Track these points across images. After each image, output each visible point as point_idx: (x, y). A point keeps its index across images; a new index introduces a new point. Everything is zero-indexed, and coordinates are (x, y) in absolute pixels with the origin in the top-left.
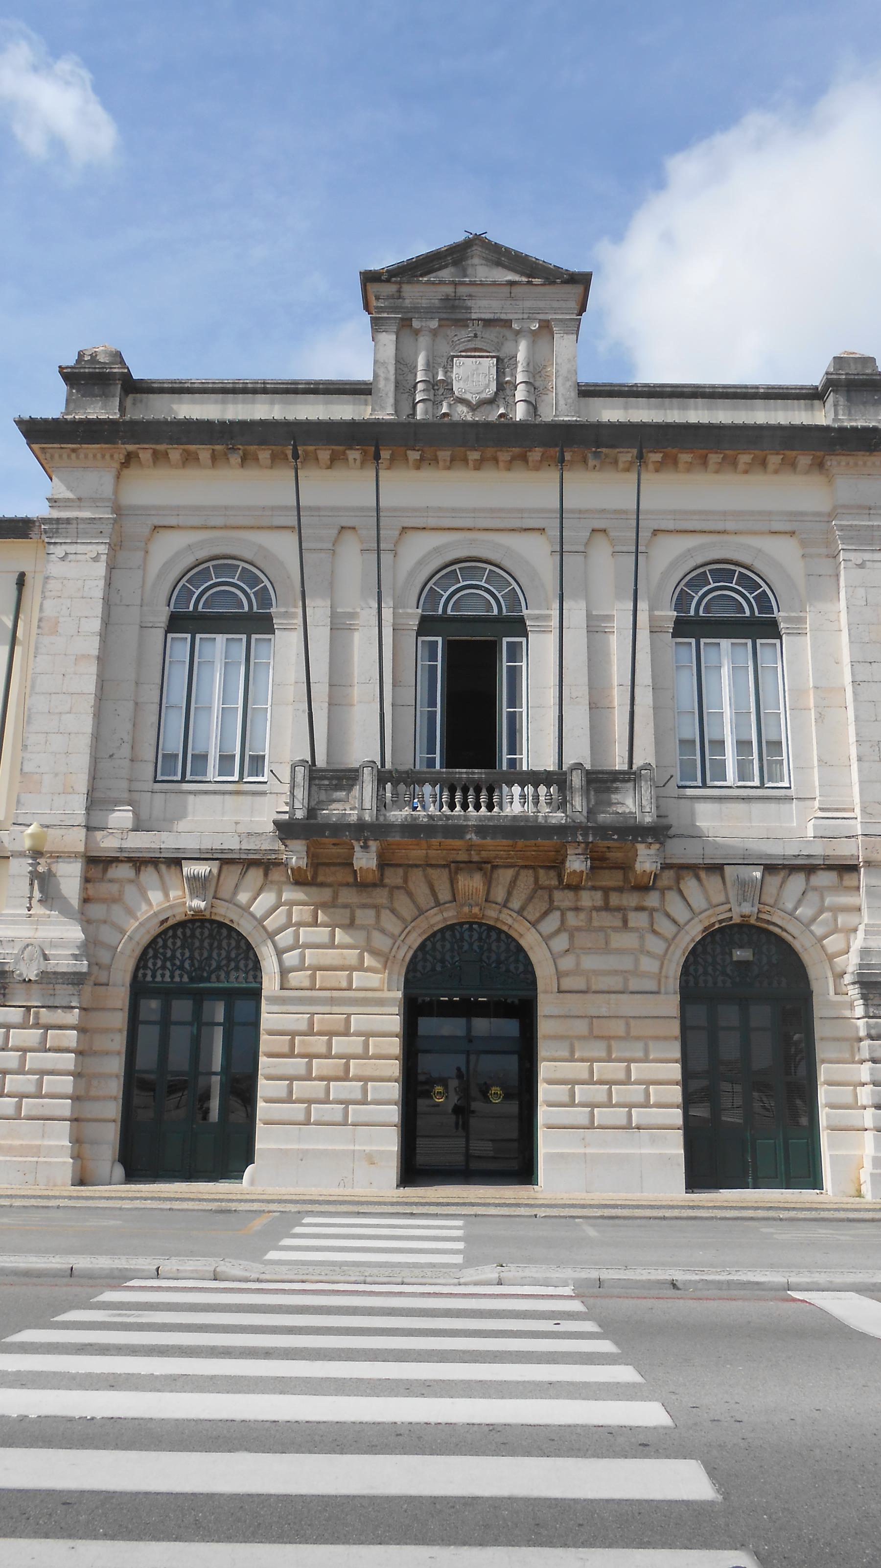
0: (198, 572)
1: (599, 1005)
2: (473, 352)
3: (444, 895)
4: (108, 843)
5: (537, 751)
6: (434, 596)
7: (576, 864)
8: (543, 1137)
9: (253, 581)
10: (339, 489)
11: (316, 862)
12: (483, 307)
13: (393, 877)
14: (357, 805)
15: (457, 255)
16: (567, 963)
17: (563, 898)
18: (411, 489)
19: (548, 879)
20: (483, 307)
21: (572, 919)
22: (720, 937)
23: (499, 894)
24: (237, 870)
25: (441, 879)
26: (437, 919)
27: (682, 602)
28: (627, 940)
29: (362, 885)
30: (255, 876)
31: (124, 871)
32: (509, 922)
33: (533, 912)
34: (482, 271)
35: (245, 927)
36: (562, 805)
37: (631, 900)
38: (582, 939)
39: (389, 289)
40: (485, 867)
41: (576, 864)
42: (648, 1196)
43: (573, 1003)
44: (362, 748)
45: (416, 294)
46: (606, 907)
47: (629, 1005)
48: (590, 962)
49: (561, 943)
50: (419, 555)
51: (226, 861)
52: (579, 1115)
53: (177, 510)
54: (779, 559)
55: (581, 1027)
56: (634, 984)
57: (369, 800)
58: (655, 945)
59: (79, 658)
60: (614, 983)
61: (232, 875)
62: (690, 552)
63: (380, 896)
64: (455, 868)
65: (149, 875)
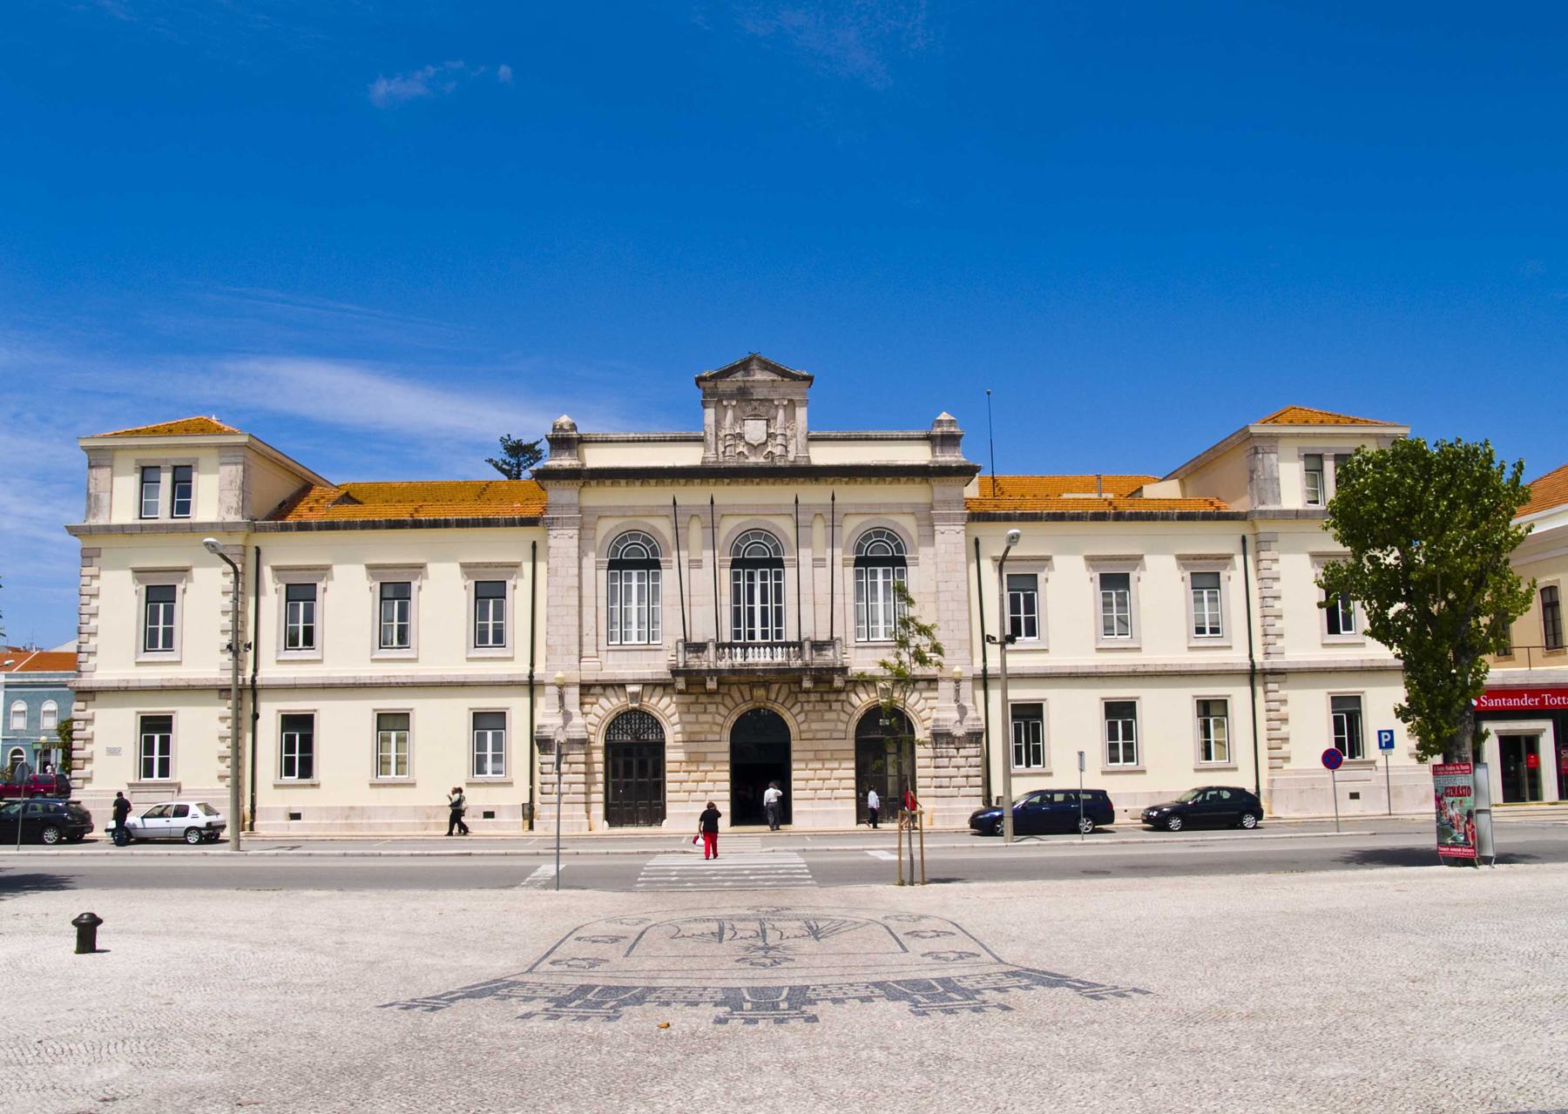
0: (745, 536)
1: (818, 745)
2: (756, 417)
3: (747, 697)
4: (589, 676)
5: (790, 635)
6: (738, 548)
7: (807, 684)
8: (794, 803)
9: (649, 542)
10: (694, 495)
11: (688, 684)
12: (759, 393)
13: (724, 689)
14: (708, 660)
15: (745, 366)
16: (804, 727)
17: (802, 697)
18: (727, 494)
19: (795, 688)
20: (759, 393)
21: (806, 707)
22: (873, 713)
23: (773, 696)
24: (650, 689)
25: (746, 689)
26: (744, 708)
27: (859, 548)
28: (833, 716)
29: (710, 693)
30: (659, 691)
31: (598, 690)
32: (777, 708)
33: (789, 704)
34: (760, 376)
35: (656, 714)
36: (800, 656)
37: (832, 697)
38: (813, 716)
39: (711, 384)
40: (766, 685)
41: (807, 684)
42: (841, 827)
43: (807, 745)
44: (702, 631)
45: (725, 385)
46: (822, 701)
47: (832, 745)
48: (814, 726)
49: (801, 718)
50: (729, 528)
51: (645, 684)
52: (810, 794)
53: (610, 507)
54: (907, 526)
55: (811, 755)
56: (835, 735)
57: (712, 657)
58: (844, 717)
59: (570, 588)
60: (825, 735)
61: (649, 690)
62: (787, 538)
63: (718, 699)
64: (752, 685)
65: (610, 692)
